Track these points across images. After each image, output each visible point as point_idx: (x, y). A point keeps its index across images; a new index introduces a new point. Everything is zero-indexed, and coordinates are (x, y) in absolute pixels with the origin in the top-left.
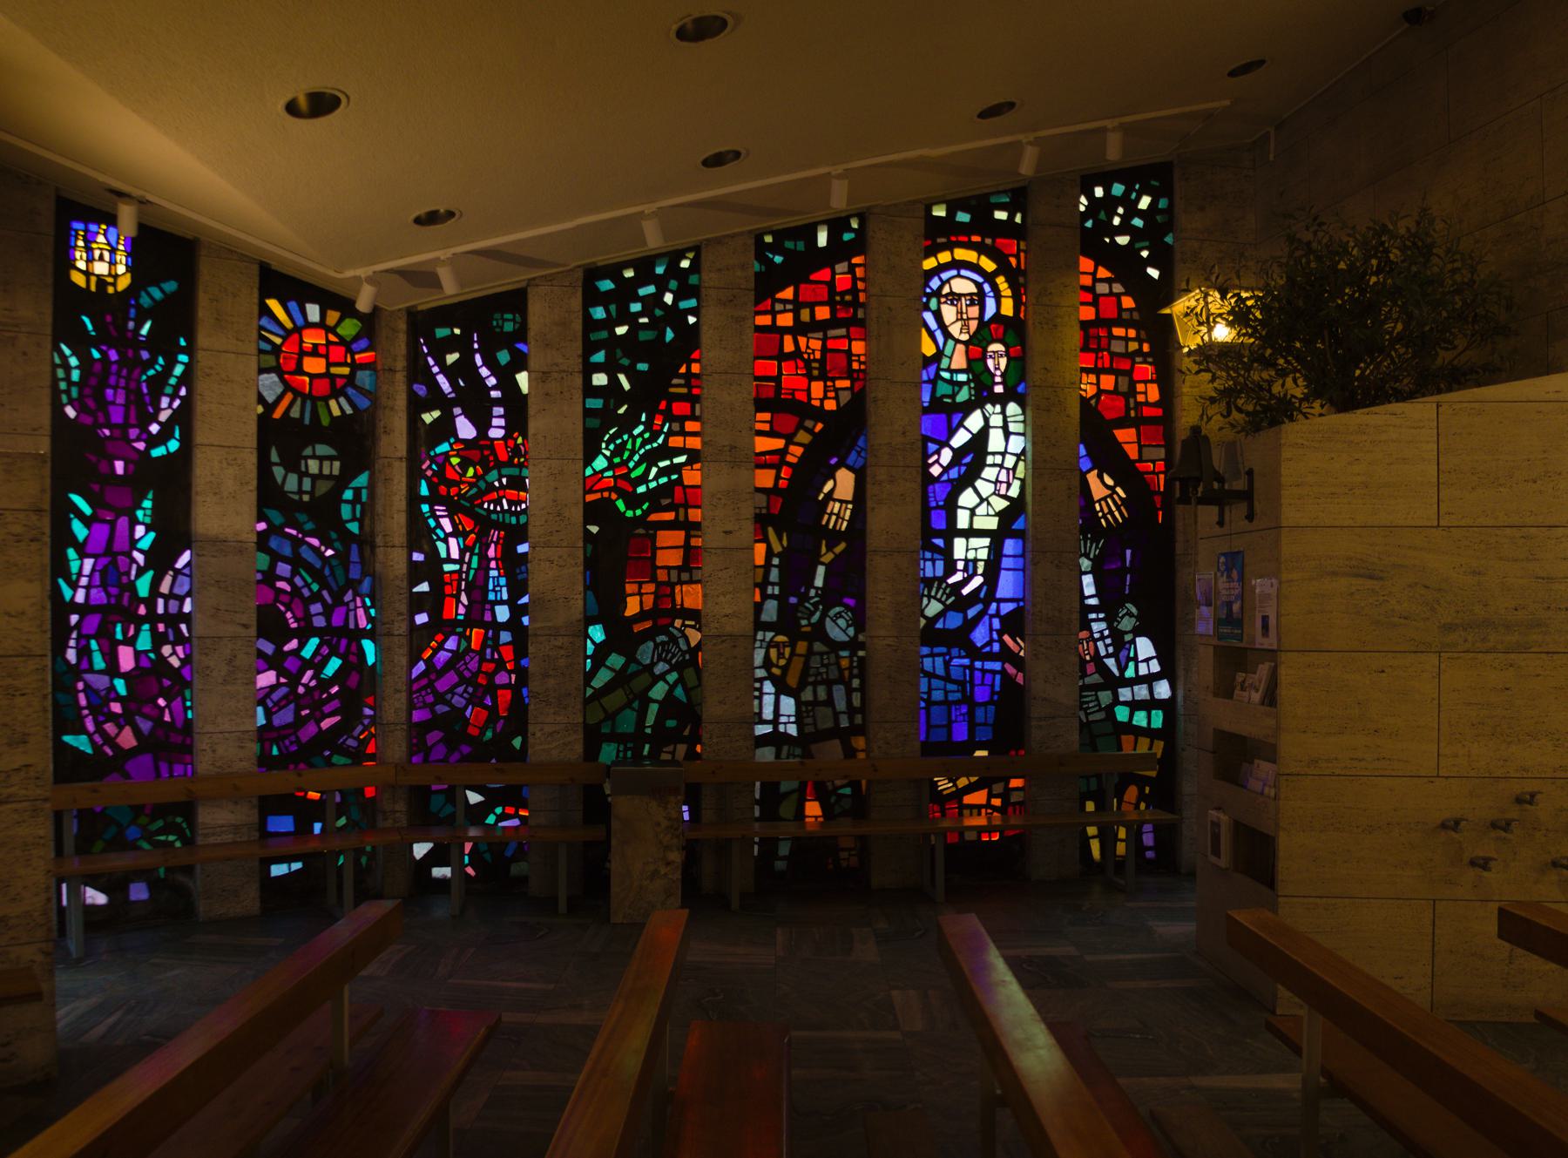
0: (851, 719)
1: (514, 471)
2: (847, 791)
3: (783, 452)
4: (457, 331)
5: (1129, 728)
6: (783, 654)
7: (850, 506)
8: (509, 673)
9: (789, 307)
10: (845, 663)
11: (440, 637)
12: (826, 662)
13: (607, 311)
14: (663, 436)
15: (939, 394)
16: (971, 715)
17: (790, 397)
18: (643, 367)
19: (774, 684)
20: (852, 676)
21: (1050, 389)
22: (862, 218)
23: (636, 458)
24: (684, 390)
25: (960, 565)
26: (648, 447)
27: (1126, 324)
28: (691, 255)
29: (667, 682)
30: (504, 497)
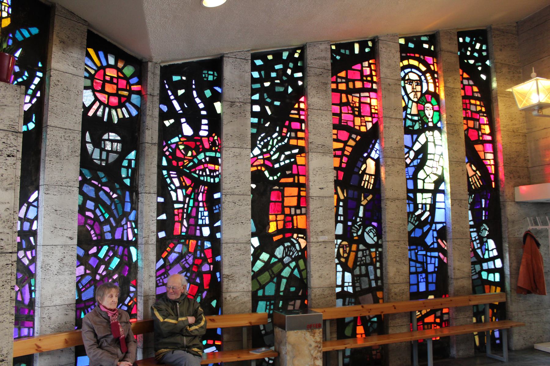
0: (376, 283)
1: (213, 154)
2: (375, 319)
3: (343, 150)
4: (184, 78)
5: (487, 282)
6: (346, 251)
7: (373, 177)
8: (210, 264)
9: (344, 80)
10: (373, 255)
11: (172, 245)
12: (365, 254)
13: (260, 74)
14: (287, 139)
15: (407, 125)
16: (427, 278)
17: (346, 124)
18: (277, 103)
19: (342, 267)
20: (376, 261)
21: (453, 125)
22: (374, 41)
23: (274, 149)
24: (297, 116)
25: (420, 206)
26: (280, 144)
27: (476, 99)
28: (299, 51)
29: (290, 267)
30: (207, 168)
